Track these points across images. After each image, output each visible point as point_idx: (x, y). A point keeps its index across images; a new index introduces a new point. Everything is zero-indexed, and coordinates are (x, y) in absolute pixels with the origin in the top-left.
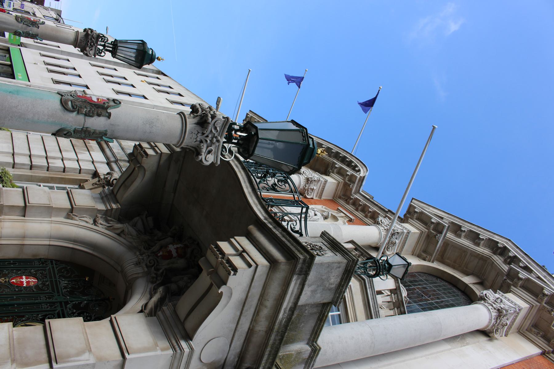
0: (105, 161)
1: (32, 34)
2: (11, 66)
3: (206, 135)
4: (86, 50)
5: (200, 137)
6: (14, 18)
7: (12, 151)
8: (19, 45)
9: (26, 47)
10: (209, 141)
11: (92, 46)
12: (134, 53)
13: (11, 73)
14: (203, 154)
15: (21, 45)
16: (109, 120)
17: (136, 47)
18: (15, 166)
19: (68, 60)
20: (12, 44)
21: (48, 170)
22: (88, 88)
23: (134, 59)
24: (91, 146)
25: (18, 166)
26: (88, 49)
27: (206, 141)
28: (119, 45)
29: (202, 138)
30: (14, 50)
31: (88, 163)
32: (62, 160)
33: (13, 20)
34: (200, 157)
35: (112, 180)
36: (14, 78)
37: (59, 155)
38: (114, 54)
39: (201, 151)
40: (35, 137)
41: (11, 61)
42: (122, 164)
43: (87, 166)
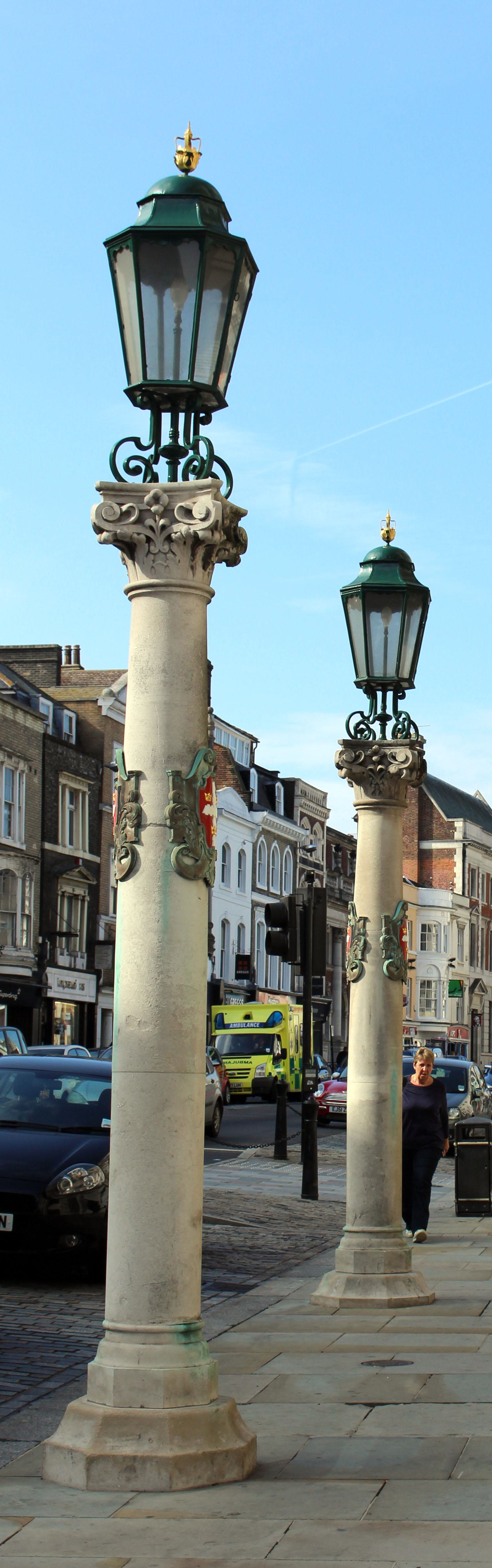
3: (150, 534)
5: (159, 545)
10: (162, 522)
11: (385, 756)
12: (387, 618)
14: (192, 529)
16: (146, 773)
23: (396, 617)
26: (393, 769)
27: (164, 527)
29: (159, 539)
34: (200, 534)
38: (400, 686)
39: (188, 534)
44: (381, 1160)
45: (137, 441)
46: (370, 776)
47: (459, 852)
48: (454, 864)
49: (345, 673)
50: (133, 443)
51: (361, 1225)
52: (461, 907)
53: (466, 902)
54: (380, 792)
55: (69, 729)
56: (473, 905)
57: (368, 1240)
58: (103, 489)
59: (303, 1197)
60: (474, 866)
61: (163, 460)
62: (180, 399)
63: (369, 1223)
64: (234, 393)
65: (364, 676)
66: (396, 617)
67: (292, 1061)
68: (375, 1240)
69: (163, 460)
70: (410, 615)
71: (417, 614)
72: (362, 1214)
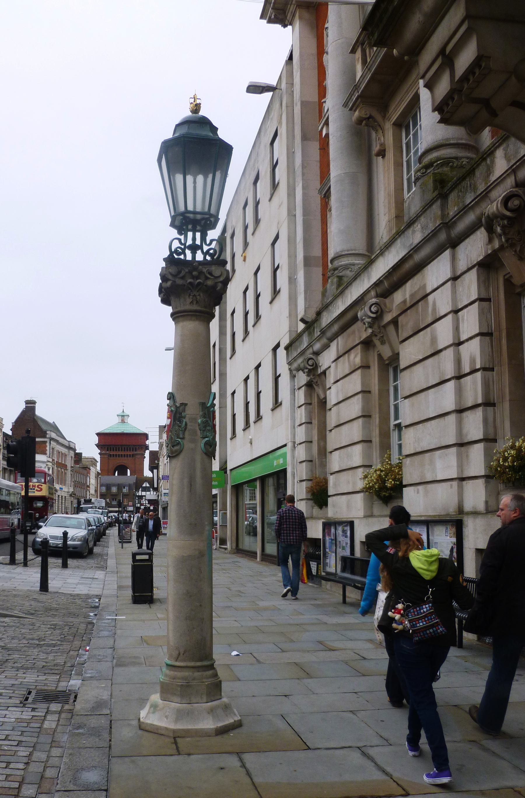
0: (447, 254)
1: (204, 416)
2: (263, 479)
4: (214, 287)
6: (174, 461)
7: (454, 450)
8: (226, 472)
9: (226, 462)
13: (275, 476)
15: (223, 468)
17: (179, 178)
18: (491, 436)
19: (233, 393)
20: (226, 483)
21: (492, 370)
22: (278, 346)
23: (210, 176)
24: (412, 296)
25: (491, 430)
26: (209, 283)
28: (182, 208)
30: (232, 480)
31: (460, 289)
32: (460, 343)
33: (178, 462)
35: (508, 213)
36: (285, 471)
37: (449, 353)
40: (408, 412)
41: (255, 480)
42: (452, 210)
43: (470, 287)
44: (200, 605)
46: (190, 289)
47: (48, 442)
48: (46, 446)
51: (184, 661)
52: (49, 461)
53: (51, 460)
54: (197, 302)
56: (53, 460)
57: (191, 673)
59: (40, 590)
60: (54, 447)
63: (192, 659)
67: (340, 547)
68: (197, 674)
70: (208, 177)
72: (185, 652)
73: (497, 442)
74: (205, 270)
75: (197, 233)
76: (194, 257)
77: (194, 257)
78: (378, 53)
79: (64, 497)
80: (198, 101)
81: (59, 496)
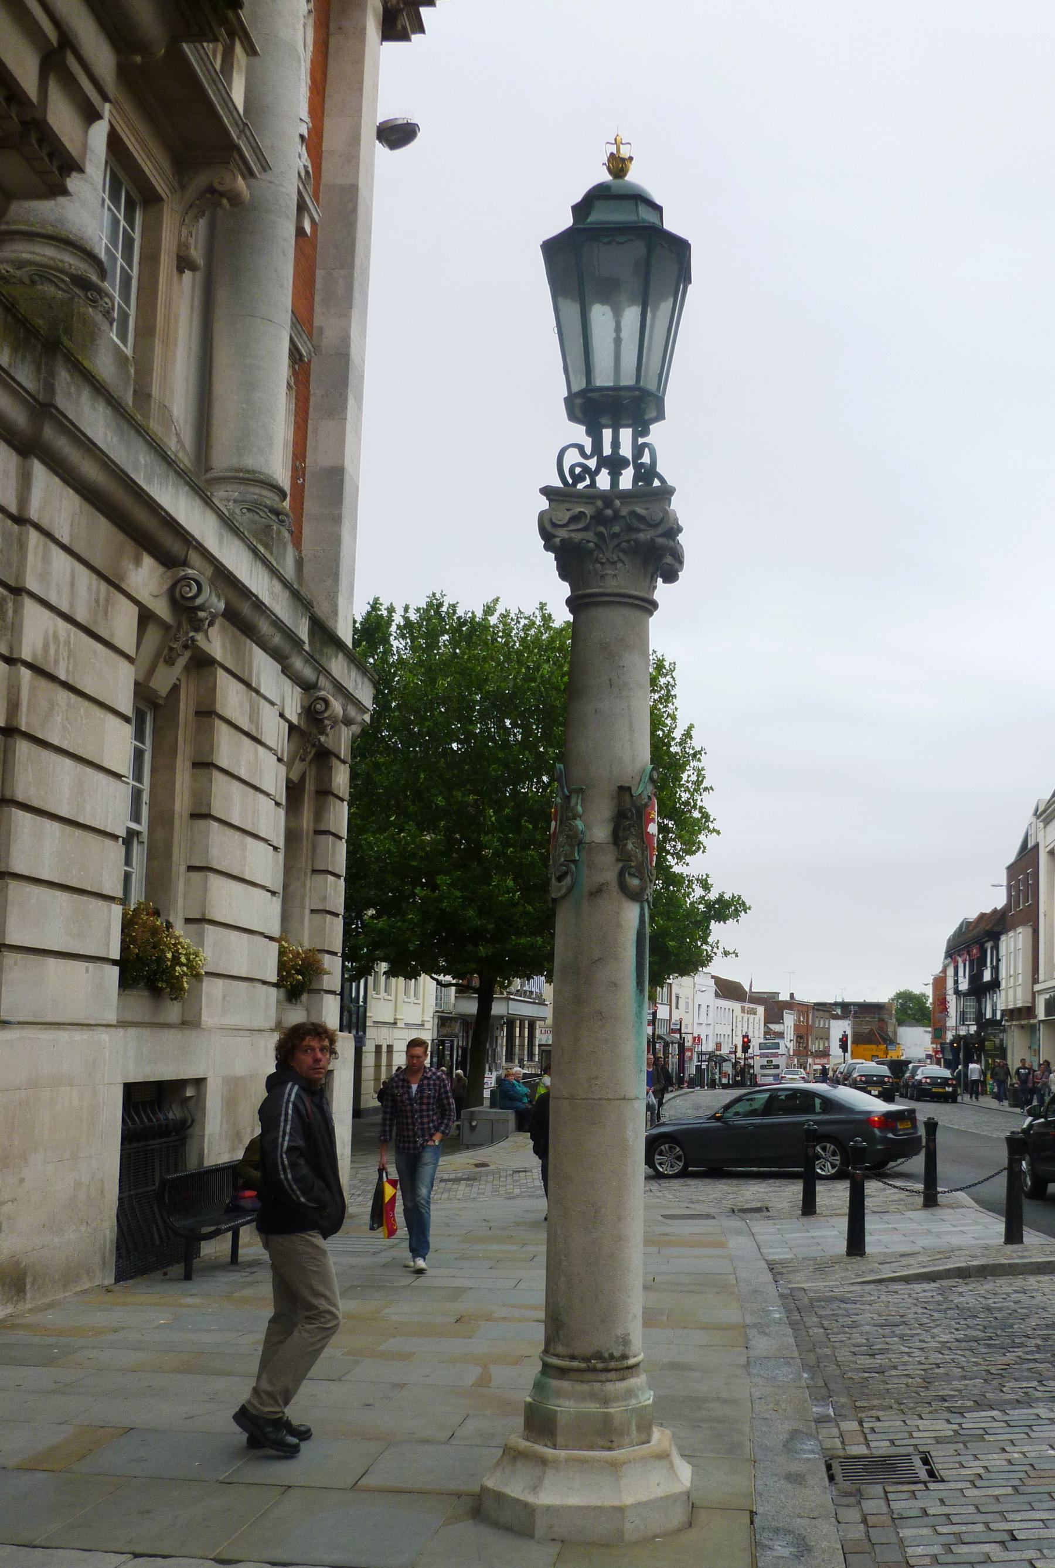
45: (581, 448)
49: (554, 387)
50: (577, 450)
55: (834, 1196)
58: (546, 491)
61: (604, 472)
62: (616, 404)
64: (675, 397)
65: (579, 385)
66: (631, 315)
69: (604, 472)
70: (656, 309)
71: (666, 306)
73: (129, 1089)
74: (624, 512)
75: (622, 430)
76: (615, 482)
77: (615, 482)
78: (208, 70)
79: (384, 1049)
80: (625, 152)
81: (378, 1048)
